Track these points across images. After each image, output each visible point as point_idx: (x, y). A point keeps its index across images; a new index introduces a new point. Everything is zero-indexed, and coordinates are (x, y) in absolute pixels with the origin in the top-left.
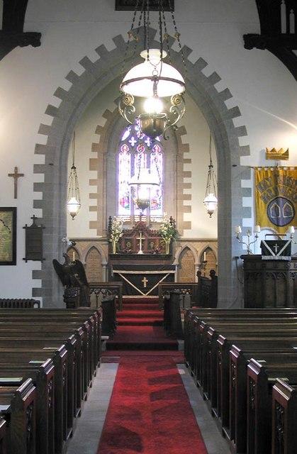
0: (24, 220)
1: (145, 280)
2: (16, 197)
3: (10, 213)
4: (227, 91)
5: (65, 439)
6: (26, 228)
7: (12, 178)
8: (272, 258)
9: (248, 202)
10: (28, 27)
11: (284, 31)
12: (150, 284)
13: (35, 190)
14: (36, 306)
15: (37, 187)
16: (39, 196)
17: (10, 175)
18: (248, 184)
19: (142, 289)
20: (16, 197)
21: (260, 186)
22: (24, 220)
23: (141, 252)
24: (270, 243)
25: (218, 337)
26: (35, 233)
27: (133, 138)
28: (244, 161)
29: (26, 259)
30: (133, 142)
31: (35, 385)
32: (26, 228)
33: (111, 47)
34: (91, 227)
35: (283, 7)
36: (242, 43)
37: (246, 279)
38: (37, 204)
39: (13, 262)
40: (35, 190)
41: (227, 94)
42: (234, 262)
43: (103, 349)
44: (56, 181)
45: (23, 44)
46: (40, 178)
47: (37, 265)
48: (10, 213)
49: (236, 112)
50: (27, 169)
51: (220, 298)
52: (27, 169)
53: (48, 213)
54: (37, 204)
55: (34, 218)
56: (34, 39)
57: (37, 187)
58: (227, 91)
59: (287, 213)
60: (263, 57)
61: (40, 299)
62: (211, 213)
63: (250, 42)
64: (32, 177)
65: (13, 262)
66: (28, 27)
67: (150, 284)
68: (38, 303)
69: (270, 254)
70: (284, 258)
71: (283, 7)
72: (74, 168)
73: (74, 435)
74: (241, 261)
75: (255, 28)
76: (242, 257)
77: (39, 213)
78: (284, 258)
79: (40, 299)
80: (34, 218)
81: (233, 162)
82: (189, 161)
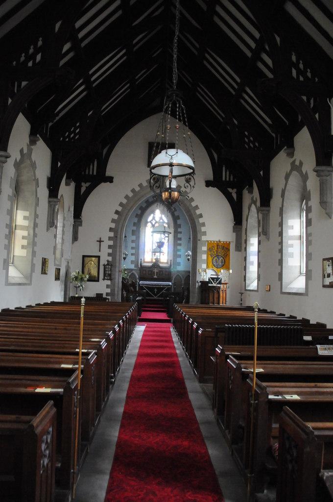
0: (103, 261)
1: (156, 290)
2: (100, 251)
3: (97, 259)
4: (197, 206)
5: (104, 401)
6: (104, 265)
7: (99, 243)
8: (213, 285)
9: (204, 257)
10: (108, 174)
11: (224, 179)
12: (158, 293)
13: (109, 248)
14: (107, 301)
15: (110, 247)
16: (110, 251)
17: (100, 238)
18: (205, 248)
19: (154, 294)
20: (100, 251)
21: (209, 249)
22: (103, 261)
23: (155, 277)
24: (213, 279)
25: (190, 320)
26: (110, 265)
27: (154, 220)
28: (204, 238)
29: (104, 279)
30: (154, 222)
31: (96, 355)
32: (104, 265)
33: (120, 209)
34: (132, 263)
35: (224, 168)
36: (204, 184)
37: (202, 292)
38: (109, 255)
39: (98, 281)
40: (109, 248)
41: (197, 207)
42: (197, 284)
43: (137, 320)
44: (118, 245)
45: (105, 182)
46: (111, 243)
47: (109, 282)
48: (97, 259)
49: (201, 216)
50: (105, 238)
51: (191, 300)
52: (105, 238)
53: (114, 258)
54: (109, 255)
55: (108, 261)
56: (110, 180)
57: (110, 247)
58: (197, 206)
59: (222, 262)
60: (214, 192)
61: (109, 297)
62: (188, 260)
63: (208, 184)
64: (107, 243)
65: (98, 281)
66: (108, 174)
67: (158, 293)
68: (109, 299)
69: (212, 283)
70: (219, 285)
71: (224, 168)
72: (125, 237)
73: (127, 353)
74: (200, 284)
75: (211, 177)
76: (200, 282)
77: (110, 259)
78: (219, 285)
79: (109, 297)
80: (108, 261)
81: (198, 238)
82: (181, 233)
